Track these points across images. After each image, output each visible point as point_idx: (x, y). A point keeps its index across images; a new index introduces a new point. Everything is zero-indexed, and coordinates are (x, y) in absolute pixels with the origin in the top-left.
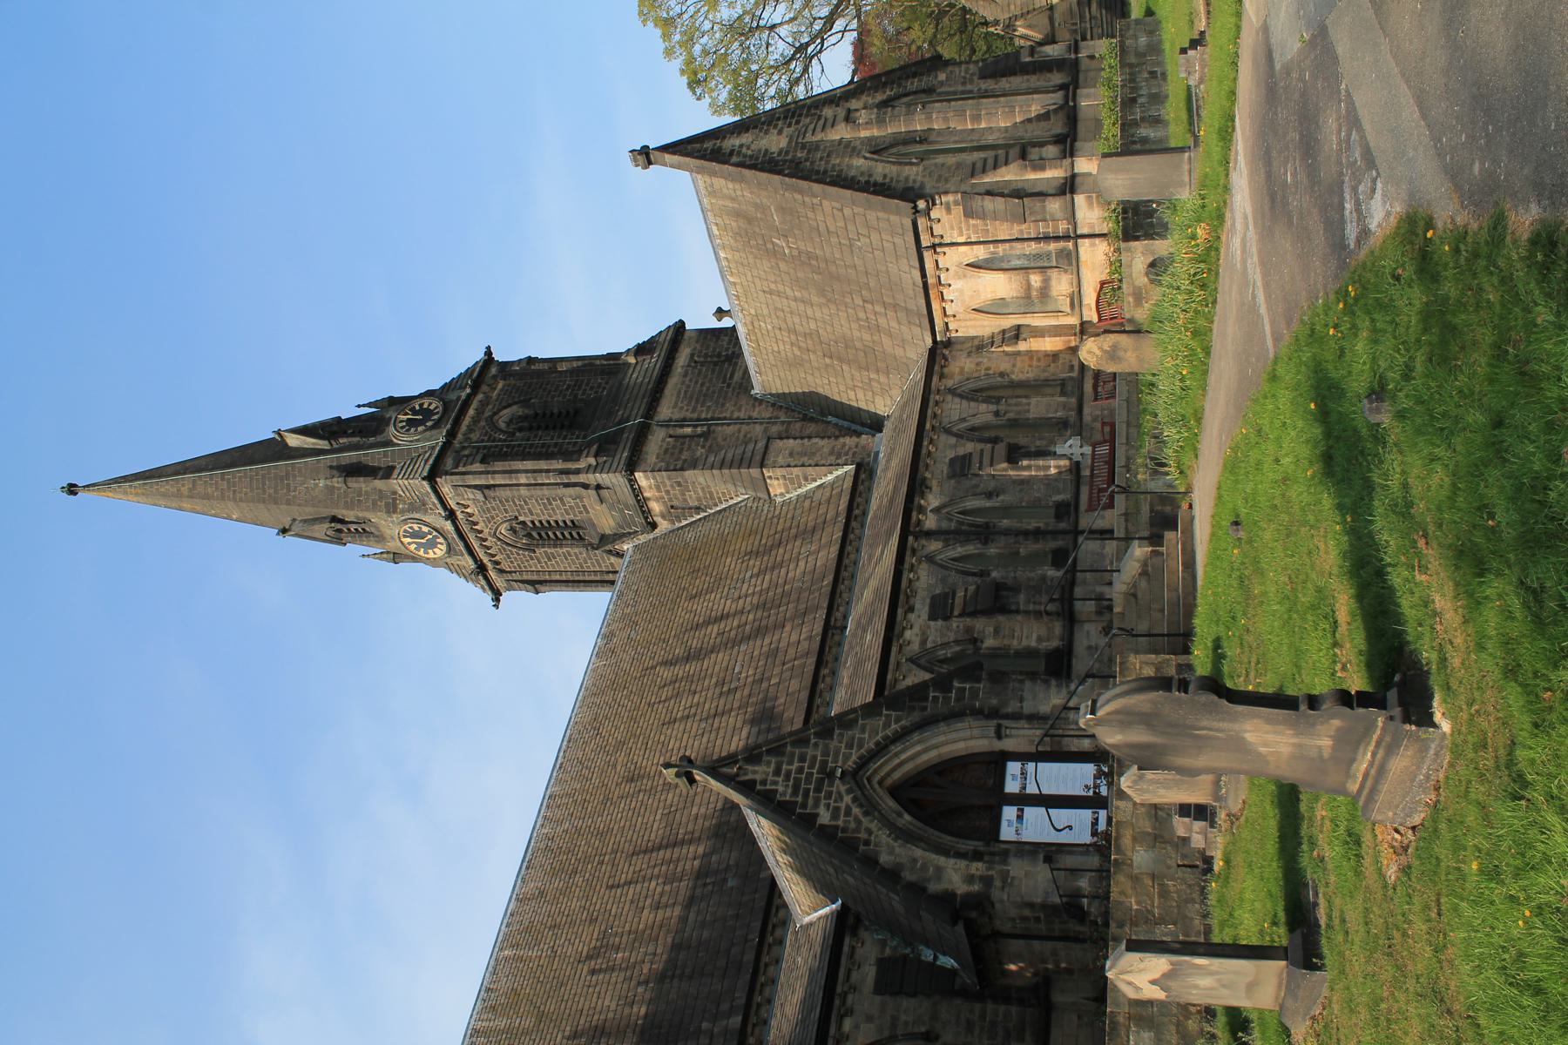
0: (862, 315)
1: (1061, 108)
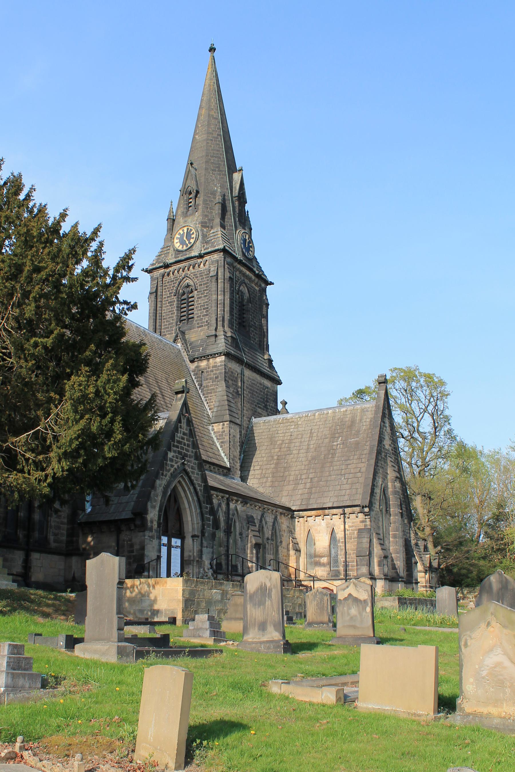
0: (304, 477)
1: (398, 575)
